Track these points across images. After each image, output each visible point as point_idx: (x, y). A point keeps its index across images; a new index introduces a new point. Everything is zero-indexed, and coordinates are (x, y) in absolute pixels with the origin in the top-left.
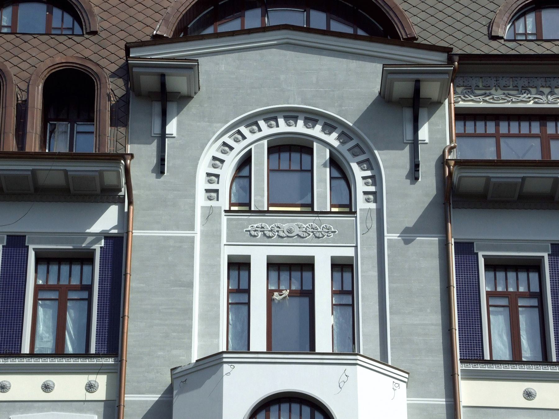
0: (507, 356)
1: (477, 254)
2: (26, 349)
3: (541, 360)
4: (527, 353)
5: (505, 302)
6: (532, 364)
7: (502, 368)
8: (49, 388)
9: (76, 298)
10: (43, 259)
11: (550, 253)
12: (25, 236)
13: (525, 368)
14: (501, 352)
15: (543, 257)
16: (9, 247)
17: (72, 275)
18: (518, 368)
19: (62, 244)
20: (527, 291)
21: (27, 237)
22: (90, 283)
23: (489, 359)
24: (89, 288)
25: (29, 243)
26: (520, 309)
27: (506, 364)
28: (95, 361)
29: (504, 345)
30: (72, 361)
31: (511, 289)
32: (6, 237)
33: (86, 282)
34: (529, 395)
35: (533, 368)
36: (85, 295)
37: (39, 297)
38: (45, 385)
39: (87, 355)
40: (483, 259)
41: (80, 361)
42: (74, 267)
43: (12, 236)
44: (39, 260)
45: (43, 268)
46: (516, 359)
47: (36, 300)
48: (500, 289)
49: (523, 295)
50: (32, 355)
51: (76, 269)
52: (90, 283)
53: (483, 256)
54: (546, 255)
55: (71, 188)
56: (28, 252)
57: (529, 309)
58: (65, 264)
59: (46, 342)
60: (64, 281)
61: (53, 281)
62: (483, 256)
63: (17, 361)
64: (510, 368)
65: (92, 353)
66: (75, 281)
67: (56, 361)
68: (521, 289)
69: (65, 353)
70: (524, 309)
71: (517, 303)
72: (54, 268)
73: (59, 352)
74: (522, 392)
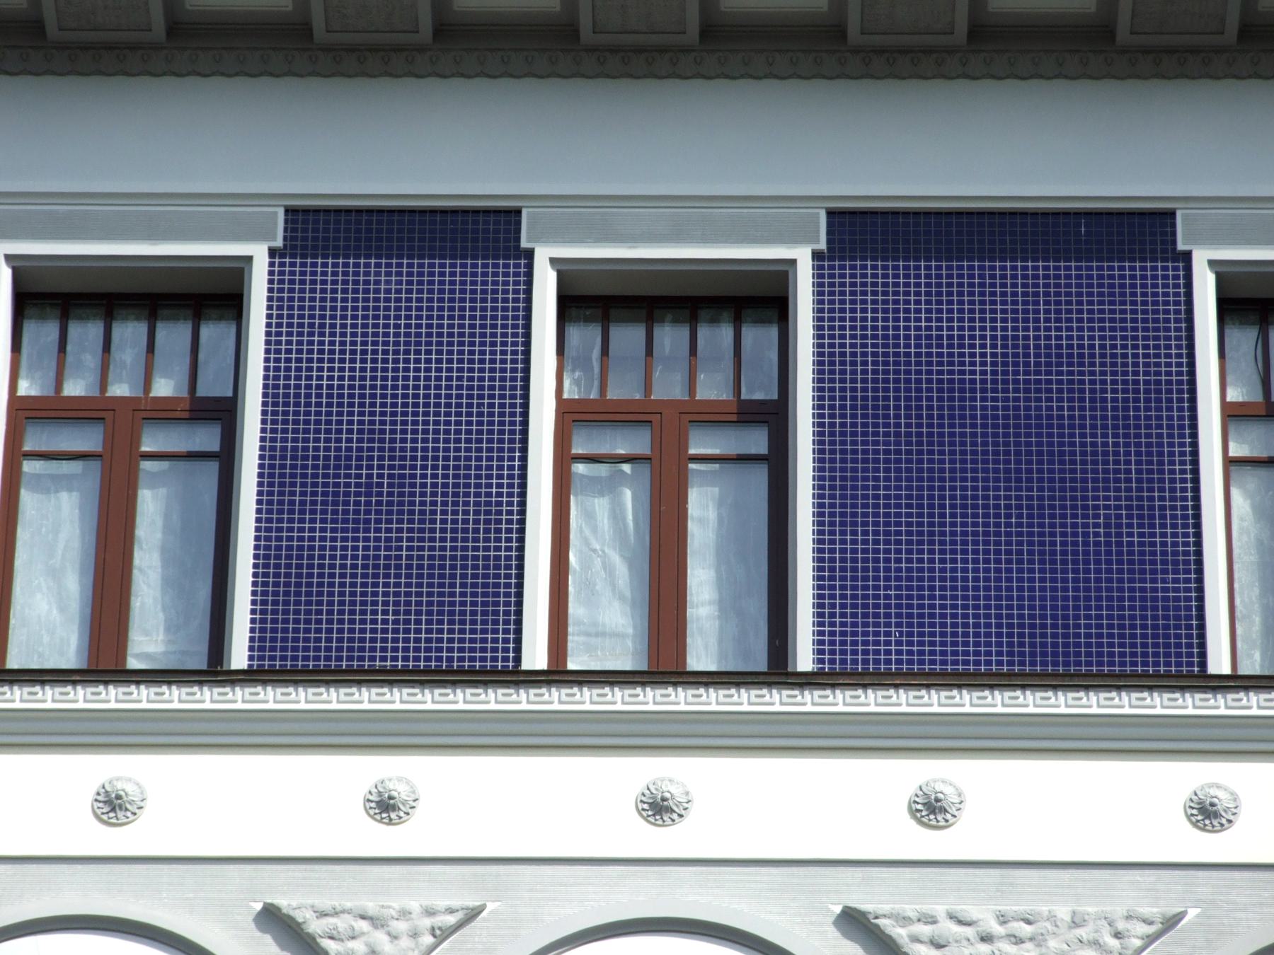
0: (67, 649)
1: (1187, 256)
2: (536, 656)
3: (763, 667)
4: (148, 642)
5: (87, 439)
6: (169, 683)
7: (48, 698)
8: (394, 808)
9: (717, 451)
10: (585, 300)
11: (279, 243)
12: (518, 212)
13: (143, 698)
14: (46, 639)
15: (793, 262)
16: (831, 259)
17: (706, 366)
18: (111, 697)
19: (705, 240)
20: (185, 394)
21: (524, 212)
22: (230, 394)
23: (1226, 670)
24: (225, 413)
25: (538, 239)
26: (146, 465)
27: (33, 682)
28: (809, 701)
29: (62, 609)
30: (713, 700)
31: (119, 390)
32: (281, 213)
33: (213, 386)
34: (931, 810)
35: (175, 698)
36: (756, 441)
37: (576, 450)
38: (1201, 802)
39: (214, 671)
40: (1211, 279)
41: (744, 700)
42: (75, 329)
43: (306, 211)
44: (573, 304)
45: (585, 336)
46: (664, 664)
47: (563, 459)
48: (74, 388)
49: (162, 413)
50: (557, 675)
51: (174, 335)
52: (230, 394)
53: (553, 261)
54: (259, 254)
55: (318, 24)
56: (530, 274)
57: (181, 465)
58: (220, 318)
59: (609, 624)
60: (669, 387)
61: (623, 389)
62: (1212, 263)
63: (492, 700)
64: (80, 698)
65: (234, 666)
66: (713, 388)
67: (650, 699)
68: (163, 388)
69: (689, 669)
70: (164, 465)
71: (135, 441)
72: (86, 333)
73: (664, 664)
74: (91, 795)
